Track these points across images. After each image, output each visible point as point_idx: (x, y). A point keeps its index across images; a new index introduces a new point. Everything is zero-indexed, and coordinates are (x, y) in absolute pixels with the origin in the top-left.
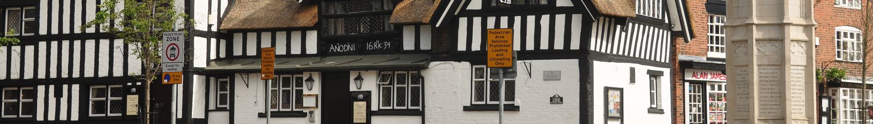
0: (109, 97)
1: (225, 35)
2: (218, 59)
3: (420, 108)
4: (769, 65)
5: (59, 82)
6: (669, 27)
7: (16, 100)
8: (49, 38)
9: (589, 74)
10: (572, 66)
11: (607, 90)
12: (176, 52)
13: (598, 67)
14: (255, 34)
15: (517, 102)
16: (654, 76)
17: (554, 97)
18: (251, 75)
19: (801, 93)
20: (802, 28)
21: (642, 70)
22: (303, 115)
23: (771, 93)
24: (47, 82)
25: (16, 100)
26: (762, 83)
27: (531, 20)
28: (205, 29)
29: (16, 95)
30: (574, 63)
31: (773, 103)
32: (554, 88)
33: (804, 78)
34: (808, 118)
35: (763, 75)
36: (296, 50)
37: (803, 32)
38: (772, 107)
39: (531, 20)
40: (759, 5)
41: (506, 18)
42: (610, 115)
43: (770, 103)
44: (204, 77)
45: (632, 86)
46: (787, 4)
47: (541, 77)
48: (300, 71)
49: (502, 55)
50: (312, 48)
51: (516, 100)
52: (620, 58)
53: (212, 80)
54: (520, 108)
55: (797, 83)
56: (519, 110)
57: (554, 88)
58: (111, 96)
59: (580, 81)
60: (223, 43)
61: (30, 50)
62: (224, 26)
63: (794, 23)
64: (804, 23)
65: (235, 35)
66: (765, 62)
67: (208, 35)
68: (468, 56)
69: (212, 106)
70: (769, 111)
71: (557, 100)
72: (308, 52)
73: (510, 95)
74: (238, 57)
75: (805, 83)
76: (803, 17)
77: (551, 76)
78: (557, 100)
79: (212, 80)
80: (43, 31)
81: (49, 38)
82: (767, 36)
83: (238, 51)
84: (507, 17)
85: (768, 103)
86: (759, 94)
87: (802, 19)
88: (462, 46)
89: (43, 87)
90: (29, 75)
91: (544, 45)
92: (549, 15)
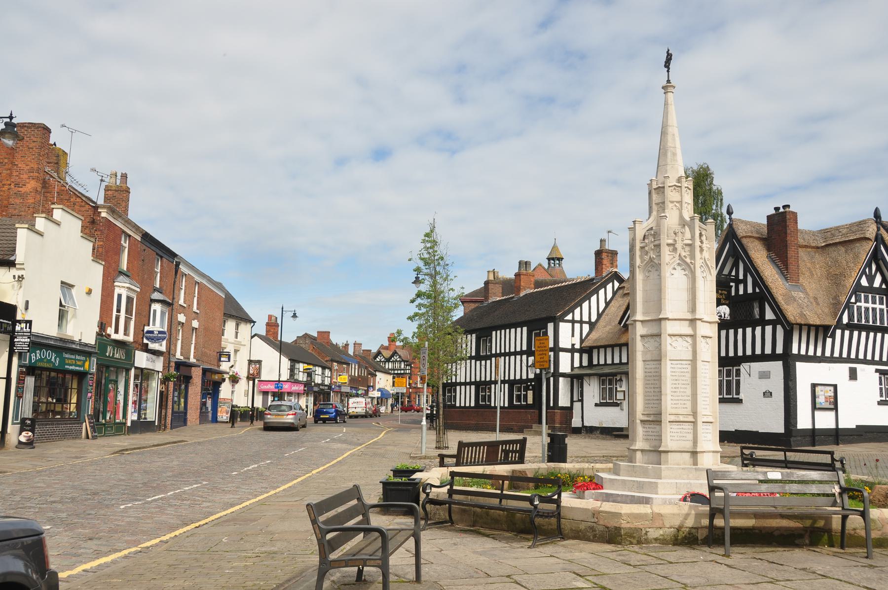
0: (522, 392)
1: (587, 350)
2: (581, 366)
4: (652, 360)
7: (520, 393)
9: (791, 373)
10: (777, 368)
11: (814, 386)
13: (801, 368)
14: (597, 350)
17: (766, 392)
18: (592, 377)
19: (686, 388)
20: (688, 322)
22: (616, 405)
23: (654, 388)
25: (520, 393)
26: (646, 378)
27: (749, 330)
28: (570, 347)
30: (780, 364)
31: (655, 398)
32: (765, 385)
33: (690, 372)
34: (693, 413)
35: (647, 370)
37: (689, 327)
38: (655, 402)
39: (749, 330)
40: (646, 302)
41: (741, 329)
42: (818, 406)
43: (652, 398)
44: (569, 379)
45: (853, 382)
46: (665, 299)
47: (757, 376)
48: (615, 374)
49: (543, 358)
51: (740, 394)
52: (834, 360)
53: (575, 380)
54: (743, 400)
55: (680, 378)
56: (742, 402)
57: (765, 385)
58: (523, 391)
59: (784, 379)
62: (586, 344)
63: (670, 318)
64: (690, 317)
65: (594, 350)
66: (649, 357)
67: (572, 350)
69: (575, 399)
70: (652, 406)
71: (768, 394)
72: (607, 363)
74: (596, 365)
75: (692, 377)
76: (690, 312)
77: (765, 375)
78: (768, 394)
79: (575, 380)
82: (650, 332)
84: (733, 330)
85: (651, 398)
86: (644, 389)
87: (689, 313)
89: (494, 385)
91: (758, 351)
92: (771, 326)
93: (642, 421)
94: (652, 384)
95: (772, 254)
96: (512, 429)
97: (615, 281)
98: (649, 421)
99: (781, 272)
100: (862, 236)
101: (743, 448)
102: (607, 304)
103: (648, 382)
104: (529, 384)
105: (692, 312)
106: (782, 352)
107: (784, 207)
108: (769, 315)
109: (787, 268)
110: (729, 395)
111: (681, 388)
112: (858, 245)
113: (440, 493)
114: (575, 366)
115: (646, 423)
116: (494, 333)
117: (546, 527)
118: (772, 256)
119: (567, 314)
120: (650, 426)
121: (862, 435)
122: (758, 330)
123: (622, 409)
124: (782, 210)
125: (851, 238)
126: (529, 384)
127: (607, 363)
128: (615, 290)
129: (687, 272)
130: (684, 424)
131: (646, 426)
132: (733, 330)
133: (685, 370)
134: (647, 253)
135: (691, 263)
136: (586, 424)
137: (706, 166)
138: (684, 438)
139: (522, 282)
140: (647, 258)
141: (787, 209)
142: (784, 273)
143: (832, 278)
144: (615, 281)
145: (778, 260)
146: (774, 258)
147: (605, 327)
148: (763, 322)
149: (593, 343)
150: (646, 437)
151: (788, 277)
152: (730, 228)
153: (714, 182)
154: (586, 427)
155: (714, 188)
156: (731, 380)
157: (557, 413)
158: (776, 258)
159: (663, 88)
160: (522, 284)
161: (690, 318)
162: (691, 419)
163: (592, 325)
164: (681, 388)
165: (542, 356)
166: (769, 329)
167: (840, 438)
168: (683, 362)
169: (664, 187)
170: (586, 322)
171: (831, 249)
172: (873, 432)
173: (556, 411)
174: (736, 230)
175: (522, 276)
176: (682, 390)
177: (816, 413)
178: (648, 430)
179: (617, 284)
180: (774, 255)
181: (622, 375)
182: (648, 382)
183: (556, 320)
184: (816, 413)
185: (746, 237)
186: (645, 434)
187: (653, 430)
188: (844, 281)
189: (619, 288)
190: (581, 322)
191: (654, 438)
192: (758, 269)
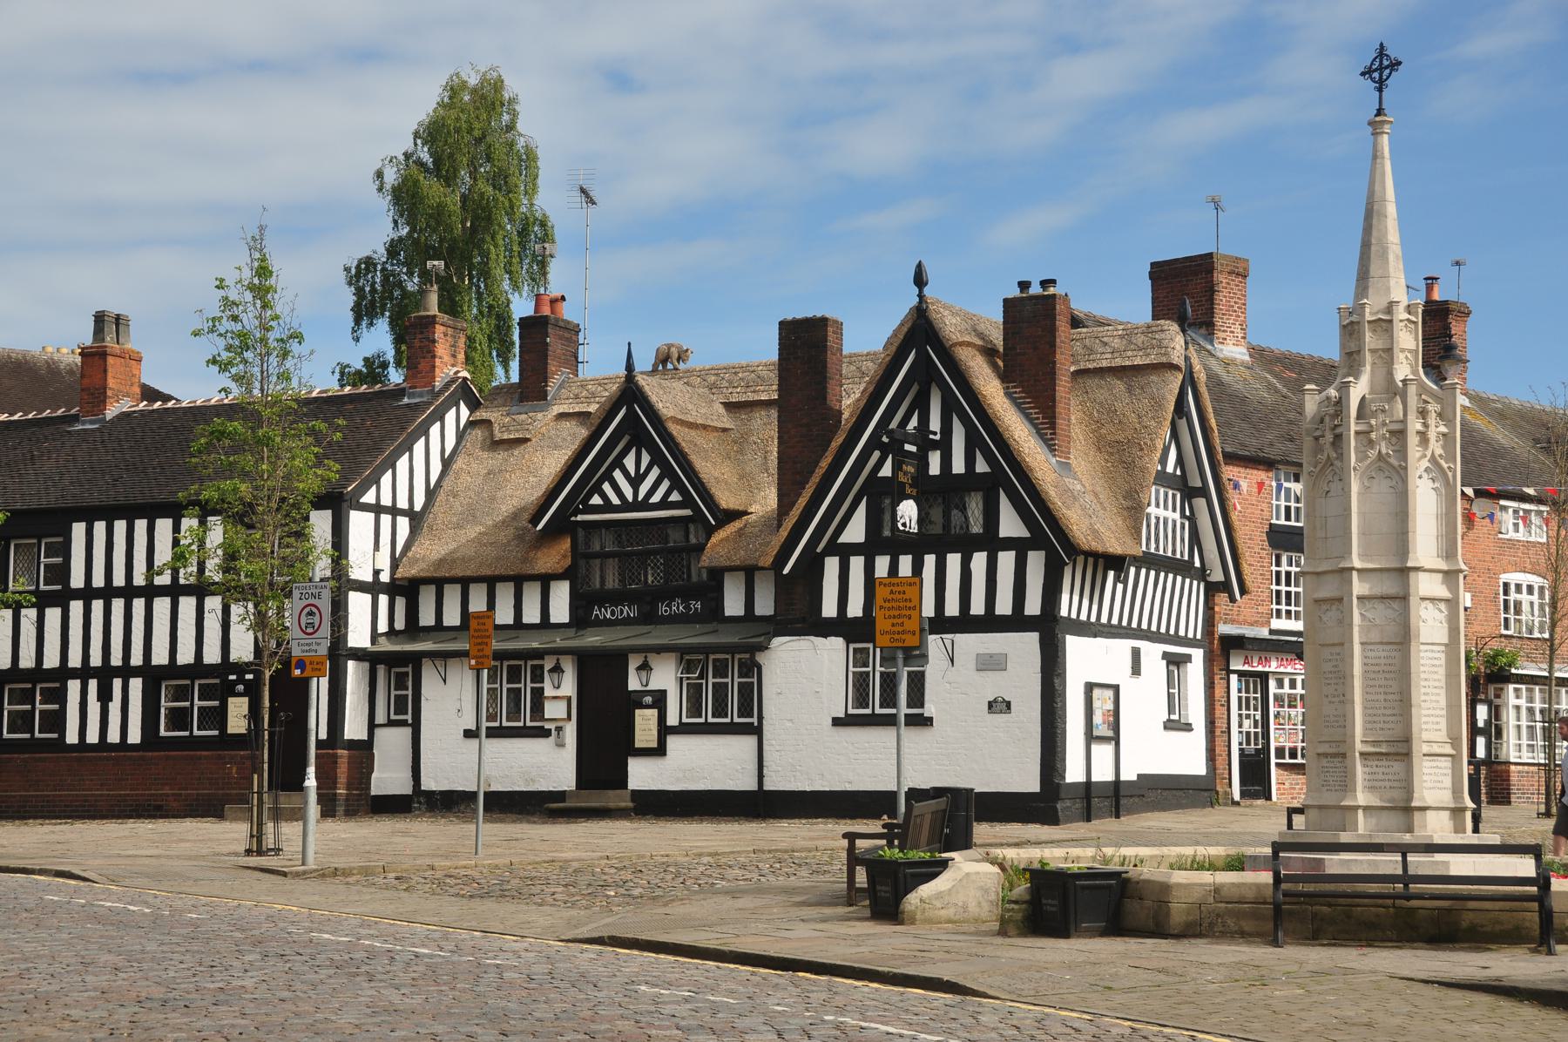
1: (404, 589)
2: (392, 632)
3: (755, 720)
4: (1381, 643)
5: (105, 674)
6: (1202, 574)
7: (28, 707)
8: (88, 594)
10: (1026, 645)
11: (1090, 687)
12: (316, 619)
13: (1075, 646)
15: (929, 709)
16: (1175, 662)
17: (995, 701)
18: (450, 662)
19: (1438, 694)
21: (1152, 653)
23: (1385, 693)
24: (85, 673)
25: (28, 707)
27: (954, 561)
28: (369, 578)
29: (28, 697)
32: (994, 684)
35: (1370, 661)
36: (532, 615)
37: (1442, 584)
39: (954, 561)
41: (910, 557)
42: (1096, 733)
43: (1383, 711)
44: (366, 665)
47: (972, 665)
48: (539, 654)
50: (560, 611)
51: (926, 706)
53: (381, 671)
56: (932, 725)
57: (994, 684)
59: (1042, 672)
60: (400, 603)
61: (53, 615)
66: (1375, 636)
67: (373, 588)
68: (842, 627)
69: (380, 718)
71: (999, 706)
72: (553, 620)
73: (917, 697)
74: (427, 629)
76: (1442, 557)
77: (991, 664)
78: (999, 706)
79: (381, 671)
80: (77, 581)
81: (88, 594)
82: (1377, 591)
83: (427, 618)
84: (910, 557)
85: (1379, 712)
88: (829, 609)
89: (78, 682)
90: (51, 660)
91: (978, 607)
92: (1014, 552)
93: (1361, 754)
94: (1380, 686)
95: (1013, 387)
96: (159, 808)
97: (462, 402)
98: (1381, 754)
99: (1038, 432)
100: (1164, 360)
101: (851, 837)
102: (447, 463)
103: (1371, 683)
104: (232, 677)
105: (1447, 557)
106: (1039, 613)
107: (1045, 283)
108: (1010, 525)
109: (1054, 423)
110: (888, 706)
111: (1433, 694)
112: (1154, 378)
113: (1223, 885)
114: (379, 632)
115: (1370, 757)
116: (79, 529)
117: (1489, 929)
118: (1016, 392)
119: (363, 489)
120: (1379, 763)
121: (1143, 796)
122: (979, 560)
123: (561, 745)
124: (1035, 289)
125: (1138, 361)
126: (232, 677)
127: (553, 620)
128: (462, 427)
129: (1437, 485)
130: (1439, 758)
131: (1369, 763)
132: (910, 557)
133: (1436, 662)
134: (1371, 443)
135: (1449, 468)
136: (428, 784)
137: (495, 74)
138: (1439, 785)
139: (110, 375)
140: (1373, 454)
141: (1052, 290)
142: (1046, 434)
143: (1110, 450)
144: (462, 402)
145: (1029, 403)
146: (1020, 398)
147: (459, 526)
148: (992, 543)
149: (435, 570)
150: (1371, 784)
151: (1055, 445)
152: (918, 318)
153: (520, 126)
154: (430, 794)
155: (521, 142)
156: (868, 673)
157: (341, 757)
158: (1024, 398)
159: (1370, 123)
160: (111, 382)
161: (1445, 568)
162: (1448, 750)
163: (416, 519)
164: (1433, 694)
165: (900, 621)
166: (1007, 560)
167: (1123, 801)
168: (1434, 648)
169: (1391, 321)
170: (403, 513)
171: (1092, 382)
172: (1157, 789)
173: (339, 751)
174: (938, 325)
175: (110, 360)
176: (1433, 698)
177: (1095, 747)
178: (1375, 770)
179: (465, 412)
180: (1020, 392)
181: (562, 658)
182: (1371, 683)
183: (337, 503)
184: (1095, 747)
185: (962, 344)
186: (1367, 777)
187: (1386, 770)
188: (1140, 458)
189: (471, 424)
190: (394, 511)
191: (1387, 784)
192: (997, 422)
